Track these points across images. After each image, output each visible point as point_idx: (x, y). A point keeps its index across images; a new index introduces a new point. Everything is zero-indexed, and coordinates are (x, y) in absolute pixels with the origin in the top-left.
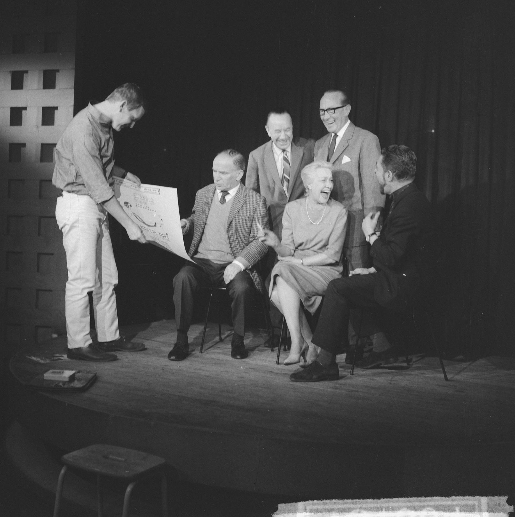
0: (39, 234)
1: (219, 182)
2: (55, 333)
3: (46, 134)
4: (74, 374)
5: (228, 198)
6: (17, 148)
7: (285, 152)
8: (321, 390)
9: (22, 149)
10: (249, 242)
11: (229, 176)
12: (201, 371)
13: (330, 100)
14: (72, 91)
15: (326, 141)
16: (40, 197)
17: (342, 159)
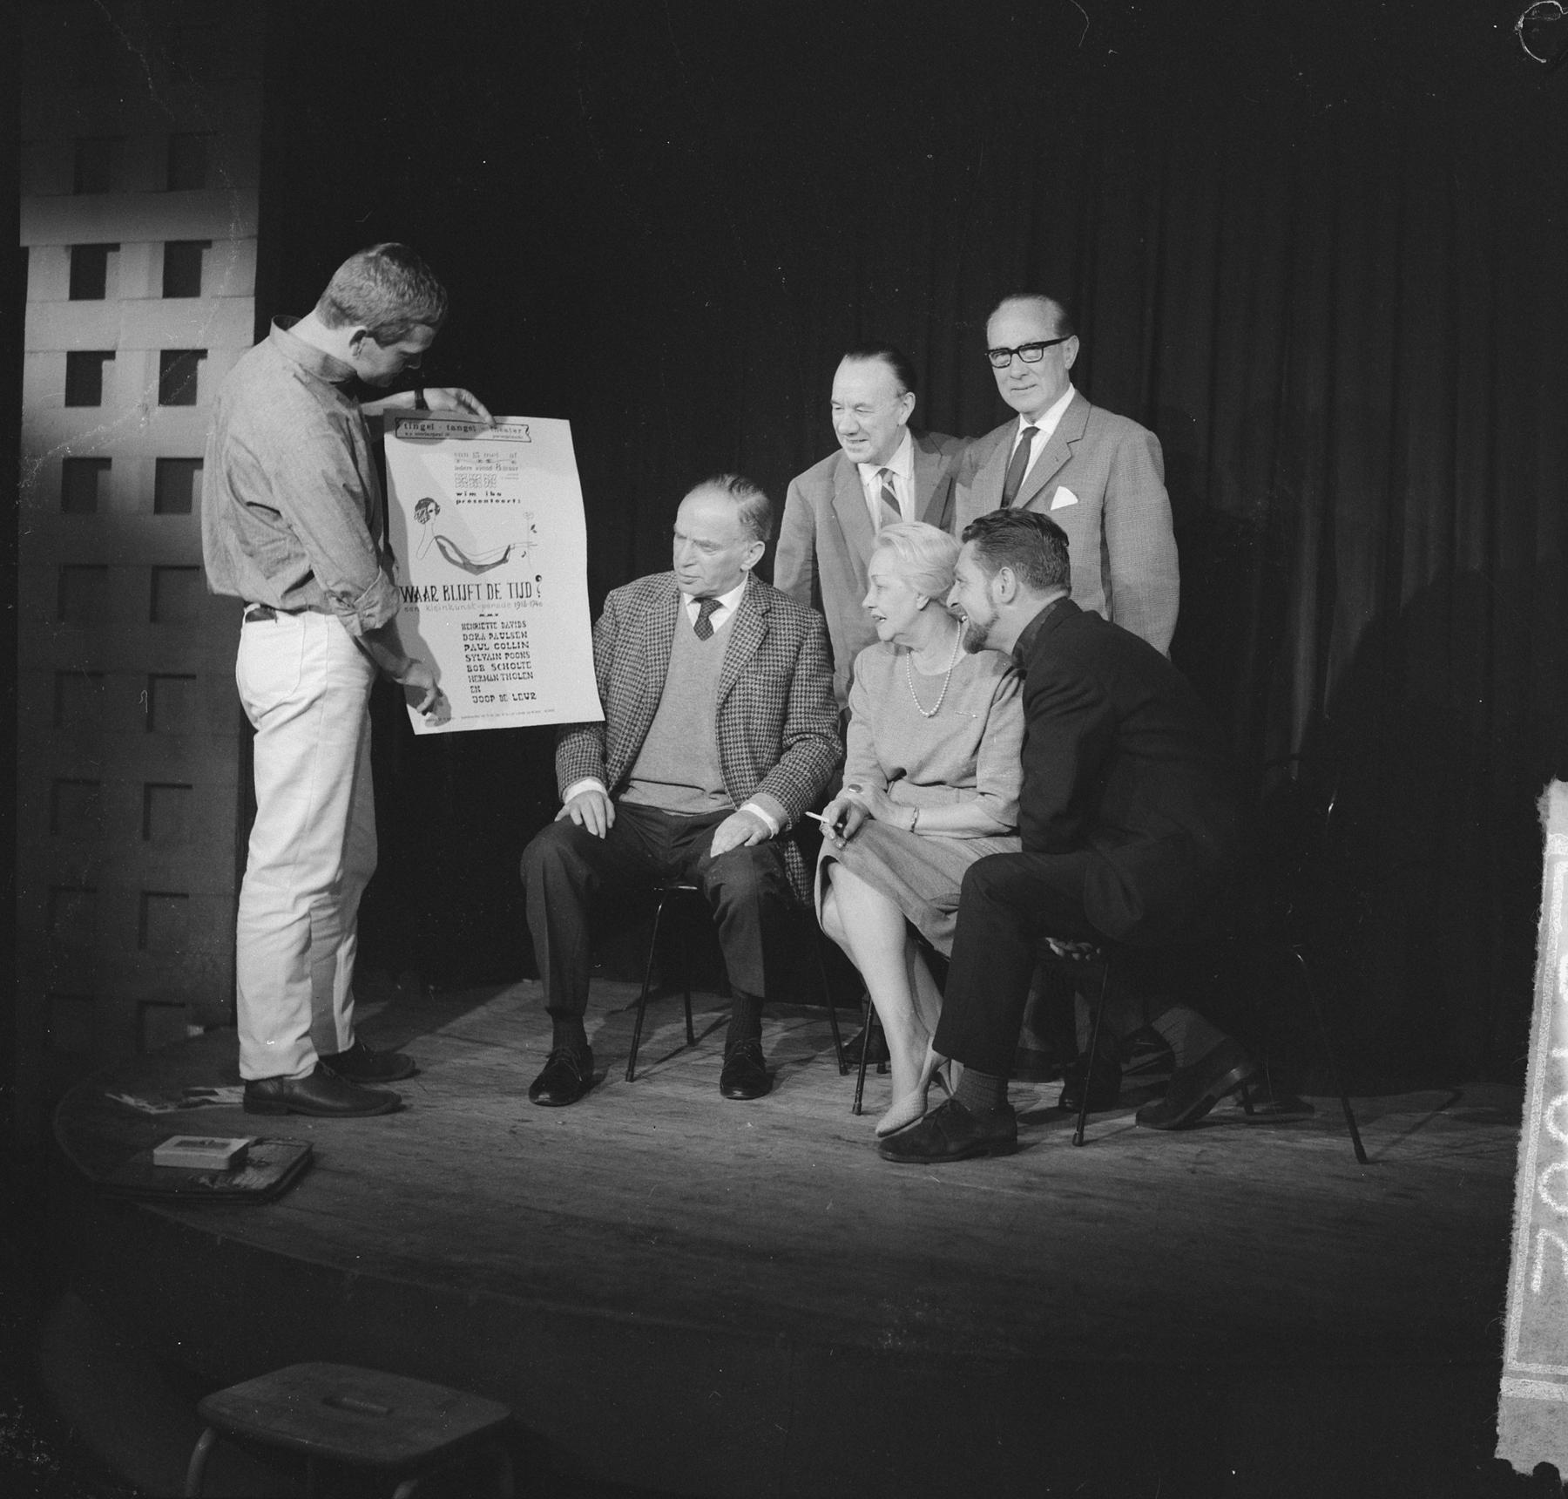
0: (150, 727)
1: (691, 571)
2: (197, 1023)
3: (172, 431)
4: (246, 1147)
5: (719, 620)
6: (86, 473)
7: (887, 476)
8: (985, 1192)
9: (102, 474)
10: (782, 750)
11: (720, 555)
12: (625, 1137)
13: (1016, 322)
14: (252, 301)
15: (1003, 444)
16: (154, 617)
17: (1051, 496)
